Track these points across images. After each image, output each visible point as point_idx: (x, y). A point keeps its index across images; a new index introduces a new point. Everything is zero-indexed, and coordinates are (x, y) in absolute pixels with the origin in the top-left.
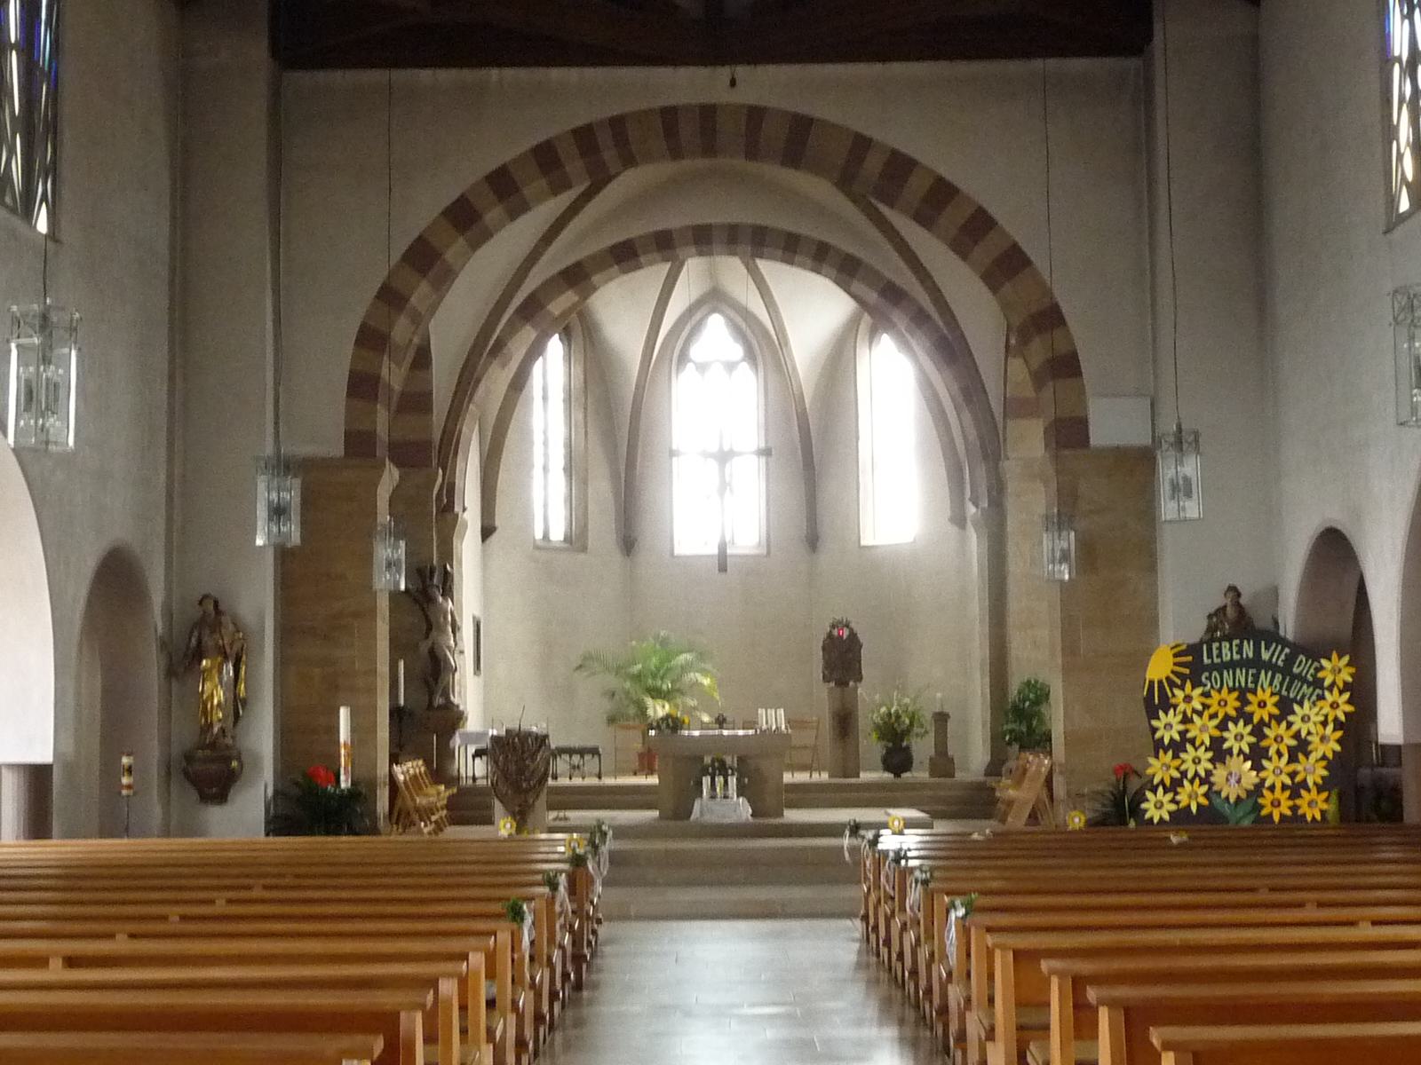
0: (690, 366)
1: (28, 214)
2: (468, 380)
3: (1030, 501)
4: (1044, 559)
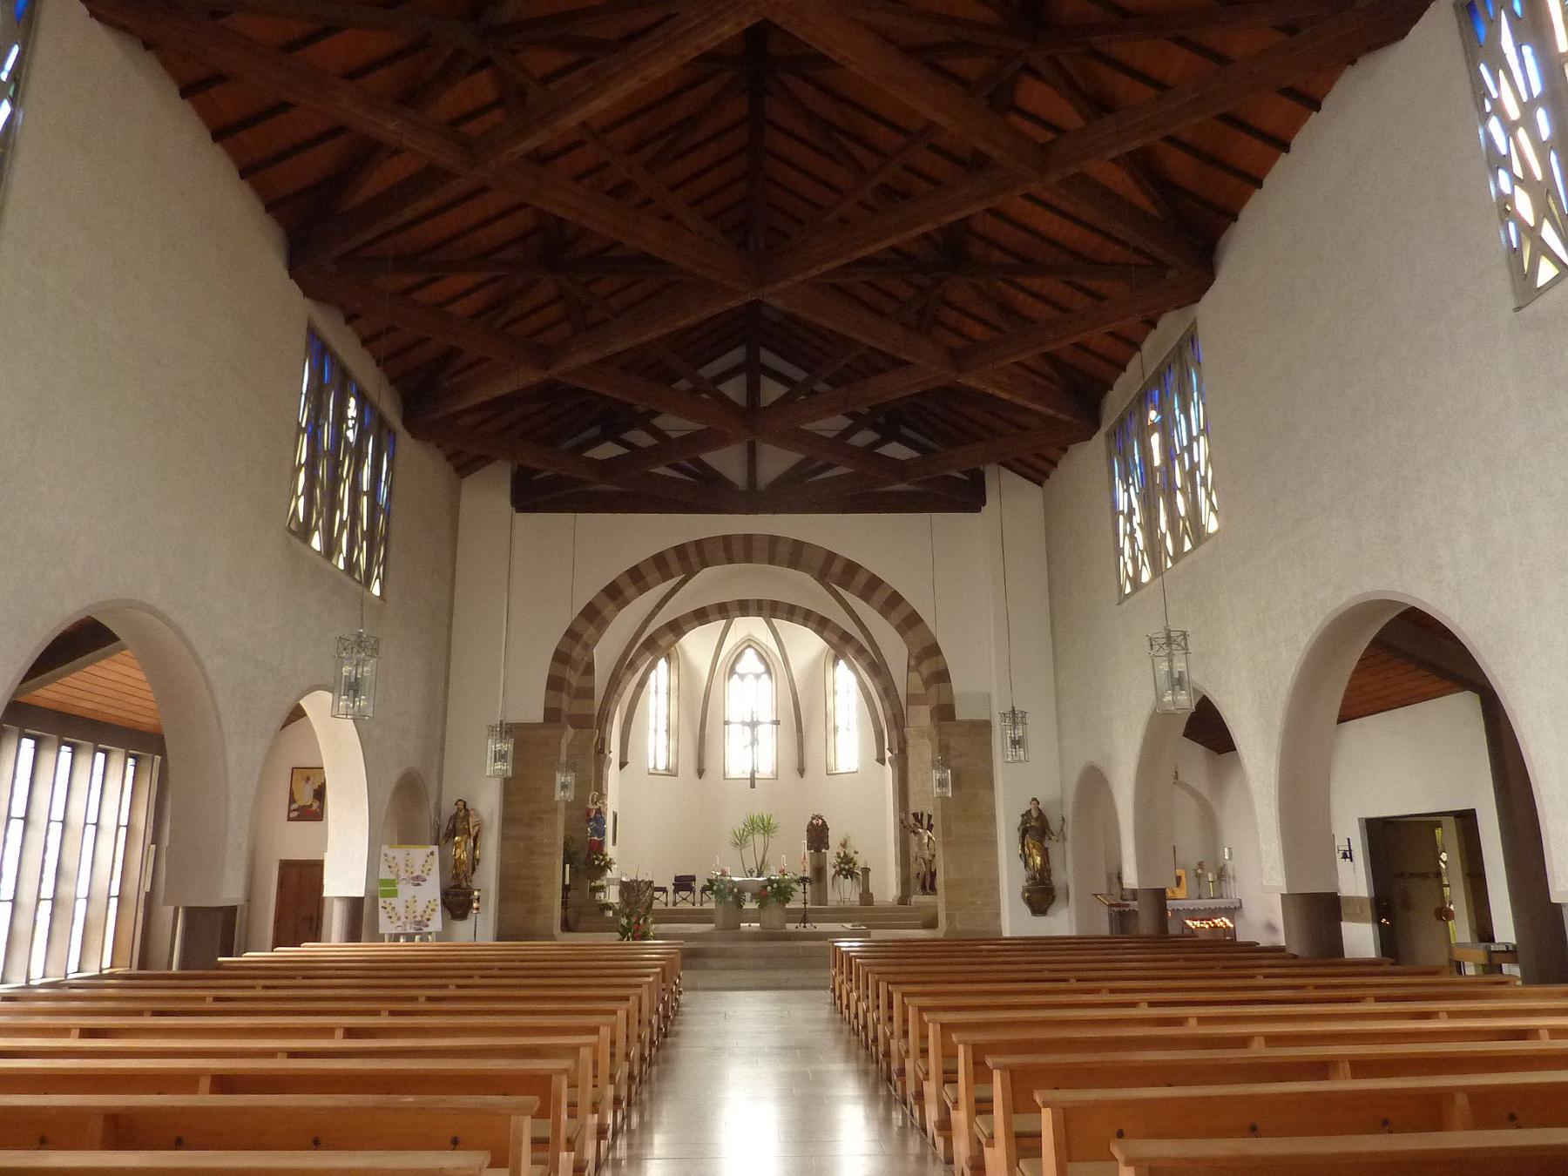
1: (367, 583)
2: (615, 683)
3: (922, 751)
4: (931, 786)
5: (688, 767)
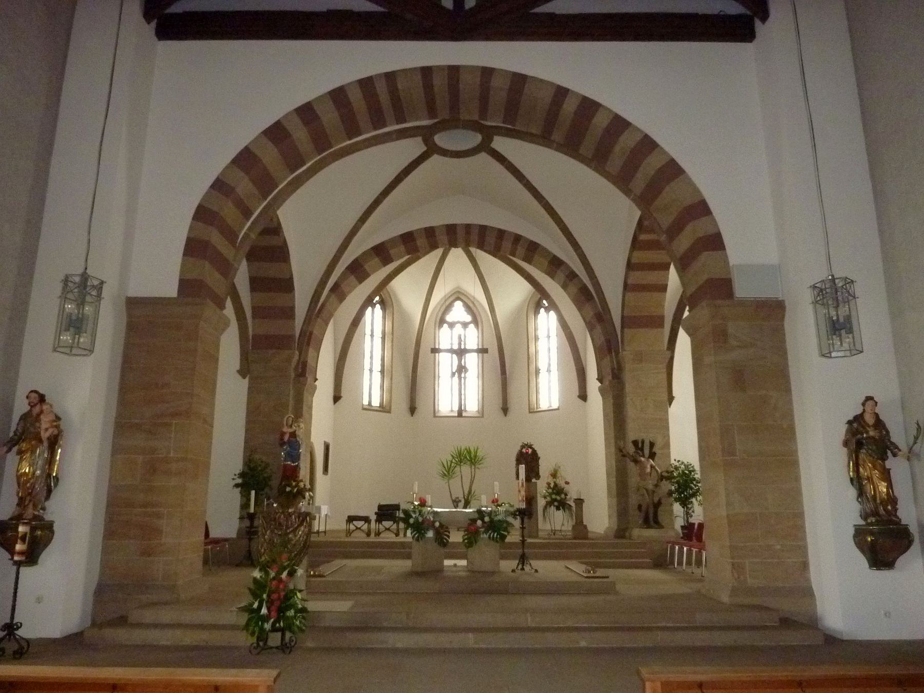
0: (445, 326)
2: (318, 312)
5: (400, 404)
